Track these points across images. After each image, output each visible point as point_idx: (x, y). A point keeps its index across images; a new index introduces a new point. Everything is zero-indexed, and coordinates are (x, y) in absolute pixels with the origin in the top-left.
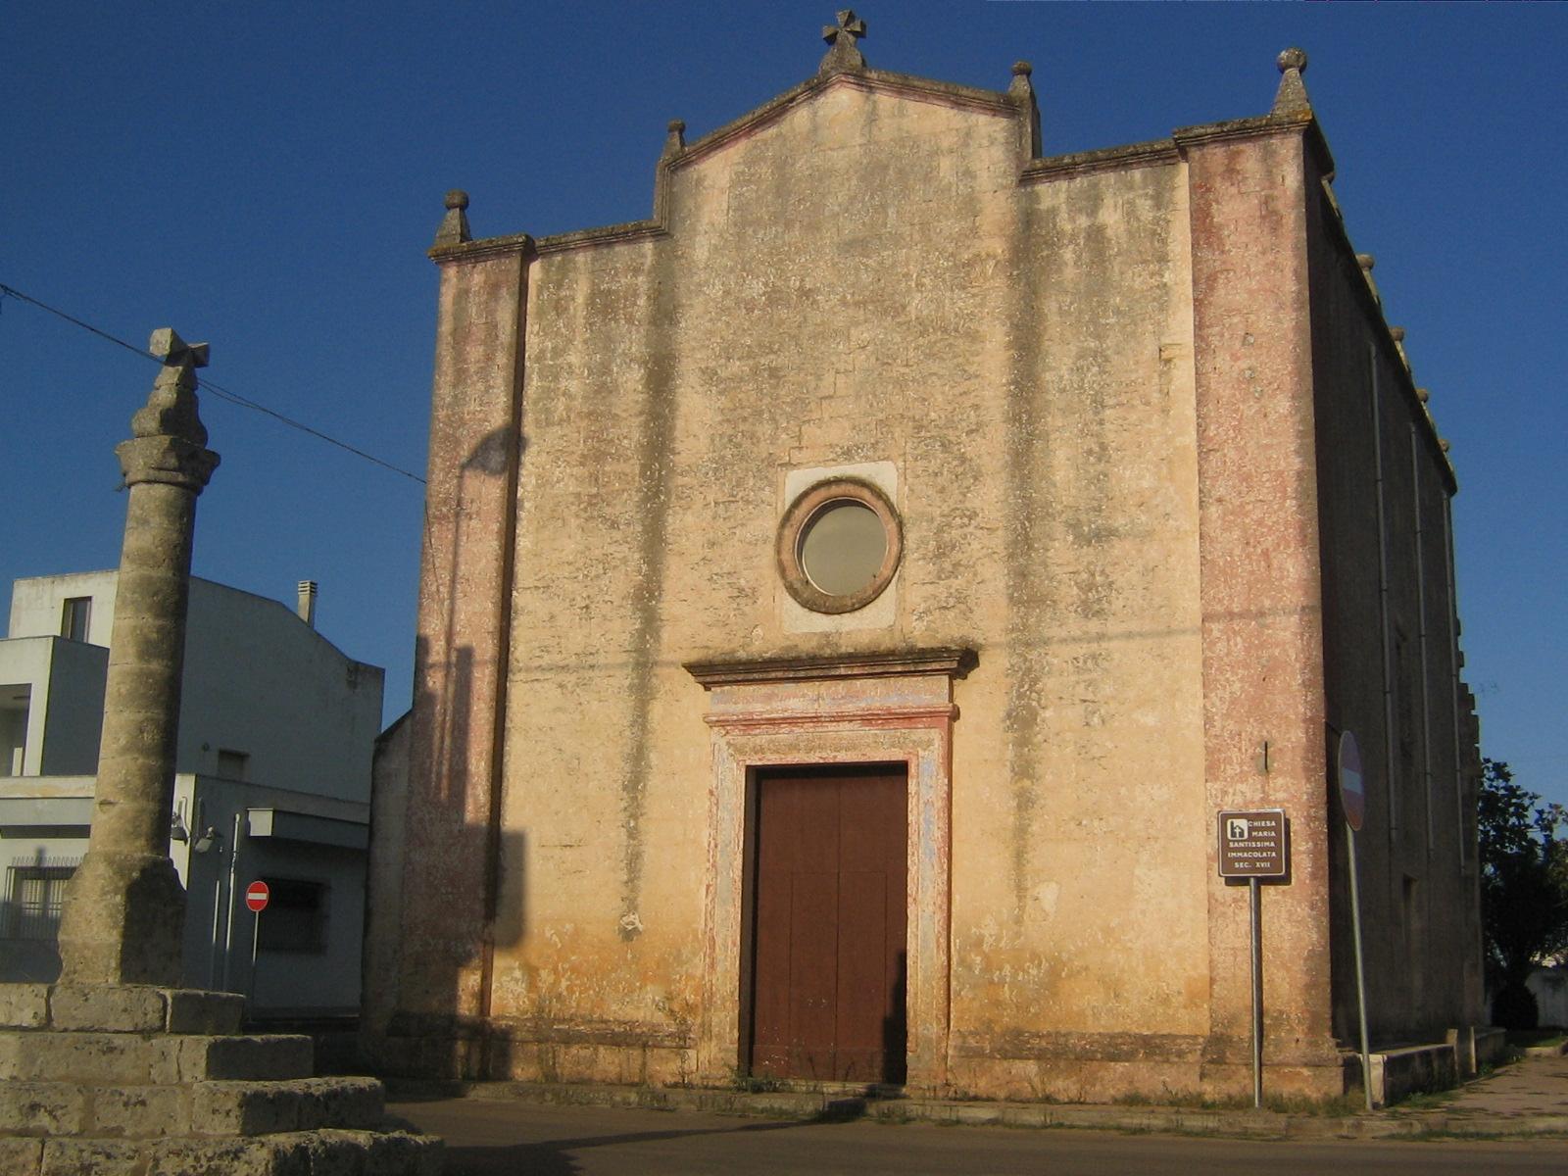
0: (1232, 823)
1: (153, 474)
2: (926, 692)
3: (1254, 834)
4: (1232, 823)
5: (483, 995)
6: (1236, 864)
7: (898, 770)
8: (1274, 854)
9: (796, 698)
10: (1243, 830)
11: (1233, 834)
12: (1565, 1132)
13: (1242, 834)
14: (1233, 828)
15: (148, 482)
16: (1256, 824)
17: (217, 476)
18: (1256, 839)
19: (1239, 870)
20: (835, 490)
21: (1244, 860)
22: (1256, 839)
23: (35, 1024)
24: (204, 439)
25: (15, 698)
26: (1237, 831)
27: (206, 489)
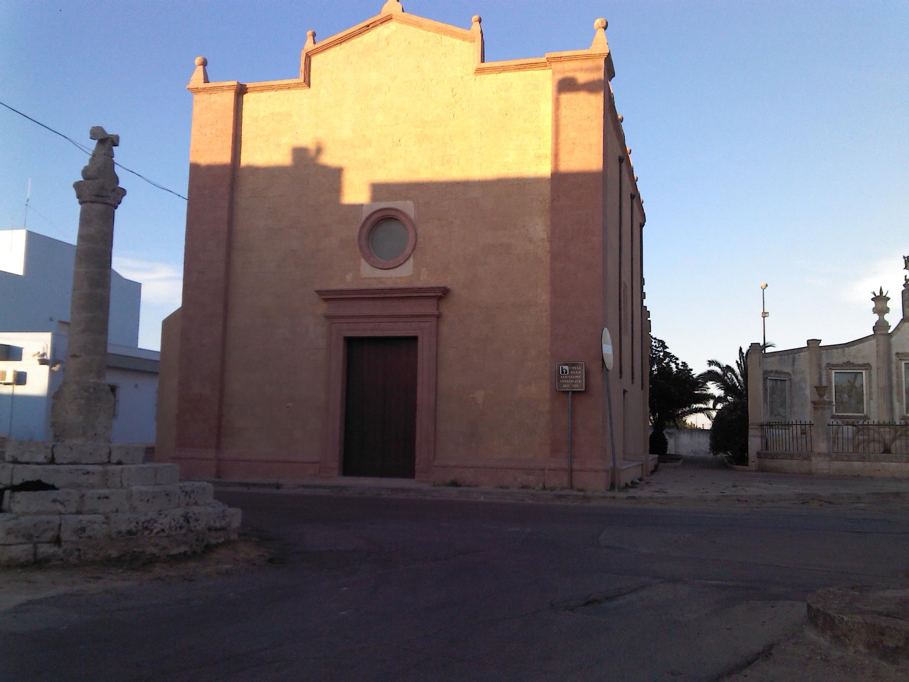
0: (562, 368)
1: (93, 198)
2: (428, 308)
3: (572, 372)
4: (562, 368)
5: (676, 446)
6: (564, 386)
7: (414, 339)
8: (580, 381)
9: (368, 308)
10: (567, 371)
11: (563, 372)
12: (908, 478)
13: (566, 372)
14: (562, 370)
15: (91, 202)
16: (573, 368)
17: (125, 199)
18: (573, 375)
19: (565, 388)
20: (384, 213)
21: (567, 383)
22: (573, 375)
23: (45, 461)
24: (118, 183)
25: (633, 383)
26: (564, 371)
27: (120, 206)
